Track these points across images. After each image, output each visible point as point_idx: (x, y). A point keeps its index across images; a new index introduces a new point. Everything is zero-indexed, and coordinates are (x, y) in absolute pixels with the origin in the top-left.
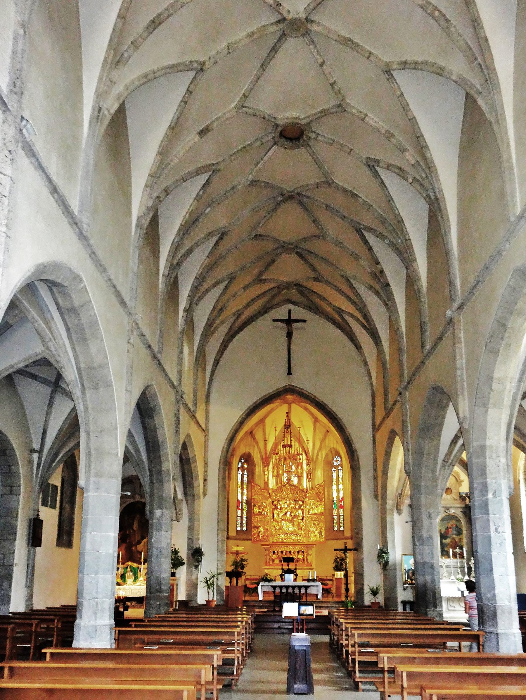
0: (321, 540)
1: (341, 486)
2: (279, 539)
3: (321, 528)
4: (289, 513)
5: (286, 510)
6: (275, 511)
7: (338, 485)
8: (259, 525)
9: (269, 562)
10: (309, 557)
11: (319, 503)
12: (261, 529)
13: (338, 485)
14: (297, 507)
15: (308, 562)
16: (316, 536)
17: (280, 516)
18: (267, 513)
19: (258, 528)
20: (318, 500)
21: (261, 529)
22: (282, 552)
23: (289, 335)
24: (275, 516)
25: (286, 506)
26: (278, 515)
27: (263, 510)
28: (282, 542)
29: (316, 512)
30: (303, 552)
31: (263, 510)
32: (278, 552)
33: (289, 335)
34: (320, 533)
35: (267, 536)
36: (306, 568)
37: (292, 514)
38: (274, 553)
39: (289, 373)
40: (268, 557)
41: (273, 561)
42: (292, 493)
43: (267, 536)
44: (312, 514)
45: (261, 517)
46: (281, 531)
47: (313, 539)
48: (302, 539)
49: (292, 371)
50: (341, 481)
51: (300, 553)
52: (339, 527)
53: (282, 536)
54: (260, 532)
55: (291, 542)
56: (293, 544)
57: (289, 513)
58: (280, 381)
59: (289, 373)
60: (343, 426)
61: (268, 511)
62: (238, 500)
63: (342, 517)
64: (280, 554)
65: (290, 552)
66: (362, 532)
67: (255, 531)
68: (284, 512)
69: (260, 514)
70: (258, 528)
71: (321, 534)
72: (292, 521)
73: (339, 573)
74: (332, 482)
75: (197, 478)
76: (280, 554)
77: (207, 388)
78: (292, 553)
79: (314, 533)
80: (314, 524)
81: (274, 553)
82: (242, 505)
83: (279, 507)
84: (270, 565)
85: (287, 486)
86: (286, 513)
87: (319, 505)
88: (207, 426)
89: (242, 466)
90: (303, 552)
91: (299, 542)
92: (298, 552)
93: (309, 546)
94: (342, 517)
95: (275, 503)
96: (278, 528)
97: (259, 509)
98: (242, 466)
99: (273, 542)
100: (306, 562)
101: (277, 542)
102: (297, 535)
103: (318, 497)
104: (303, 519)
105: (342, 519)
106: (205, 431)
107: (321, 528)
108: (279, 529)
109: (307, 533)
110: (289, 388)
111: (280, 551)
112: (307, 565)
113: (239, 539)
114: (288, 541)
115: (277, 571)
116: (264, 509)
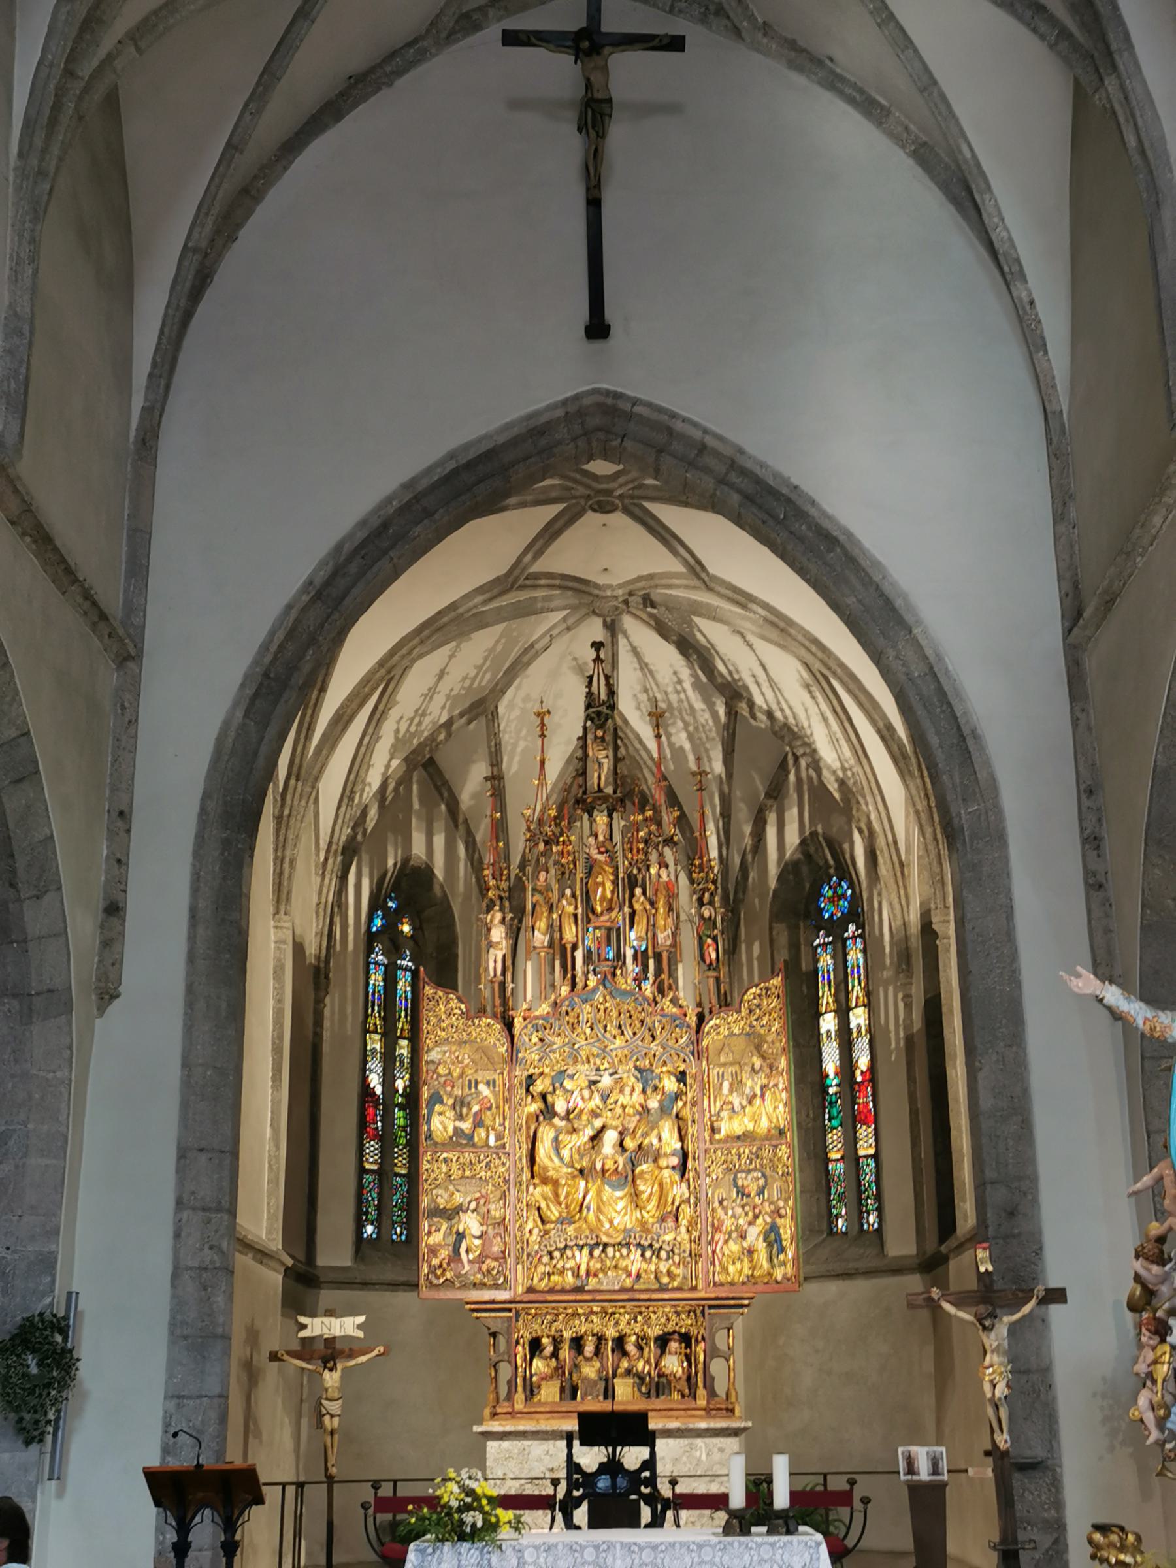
0: (779, 1274)
1: (858, 1018)
2: (562, 1272)
3: (777, 1213)
4: (611, 1137)
5: (598, 1123)
6: (546, 1135)
7: (843, 1013)
8: (459, 1198)
9: (509, 1398)
10: (717, 1367)
11: (761, 1080)
12: (470, 1223)
13: (843, 1013)
14: (653, 1104)
15: (712, 1394)
16: (751, 1252)
17: (566, 1153)
18: (499, 1137)
19: (452, 1214)
20: (757, 1063)
21: (470, 1223)
22: (577, 1343)
23: (594, 114)
24: (544, 1150)
25: (597, 1101)
26: (557, 1144)
27: (478, 1123)
28: (579, 1290)
29: (750, 1127)
30: (686, 1339)
31: (478, 1123)
32: (557, 1342)
33: (594, 114)
34: (772, 1237)
35: (502, 1257)
36: (703, 1425)
37: (630, 1144)
38: (535, 1346)
39: (597, 329)
40: (505, 1371)
41: (531, 1391)
42: (629, 1032)
43: (502, 1257)
44: (728, 1138)
45: (468, 1156)
46: (571, 1230)
47: (737, 1271)
48: (679, 1271)
49: (611, 314)
50: (857, 991)
51: (674, 1345)
52: (860, 1213)
53: (582, 1258)
54: (461, 1236)
55: (623, 1290)
56: (634, 1298)
57: (611, 1137)
58: (547, 373)
59: (597, 329)
60: (898, 603)
61: (502, 1130)
62: (366, 1091)
63: (869, 1167)
64: (565, 1353)
65: (620, 1342)
66: (1035, 1202)
67: (434, 1236)
68: (589, 1132)
69: (462, 1140)
70: (452, 1214)
71: (778, 1240)
72: (628, 1178)
73: (619, 1391)
74: (816, 1000)
75: (47, 884)
76: (565, 1353)
77: (138, 402)
78: (630, 1348)
79: (743, 1237)
80: (742, 1192)
81: (535, 1346)
82: (388, 1118)
83: (560, 1107)
84: (512, 1414)
85: (599, 997)
86: (596, 1137)
87: (764, 1087)
88: (135, 608)
89: (391, 927)
90: (686, 1339)
91: (663, 1288)
92: (663, 1342)
93: (724, 1304)
94: (869, 1167)
95: (539, 1086)
96: (554, 1213)
97: (460, 1117)
98: (391, 927)
99: (530, 1290)
100: (701, 1392)
101: (552, 1291)
102: (657, 1253)
103: (758, 1047)
104: (683, 1168)
105: (868, 1177)
106: (124, 645)
107: (777, 1213)
108: (561, 1221)
109: (705, 1236)
110: (599, 405)
111: (567, 1335)
112: (708, 1411)
113: (365, 1285)
114: (610, 1281)
115: (537, 1448)
116: (487, 1118)
